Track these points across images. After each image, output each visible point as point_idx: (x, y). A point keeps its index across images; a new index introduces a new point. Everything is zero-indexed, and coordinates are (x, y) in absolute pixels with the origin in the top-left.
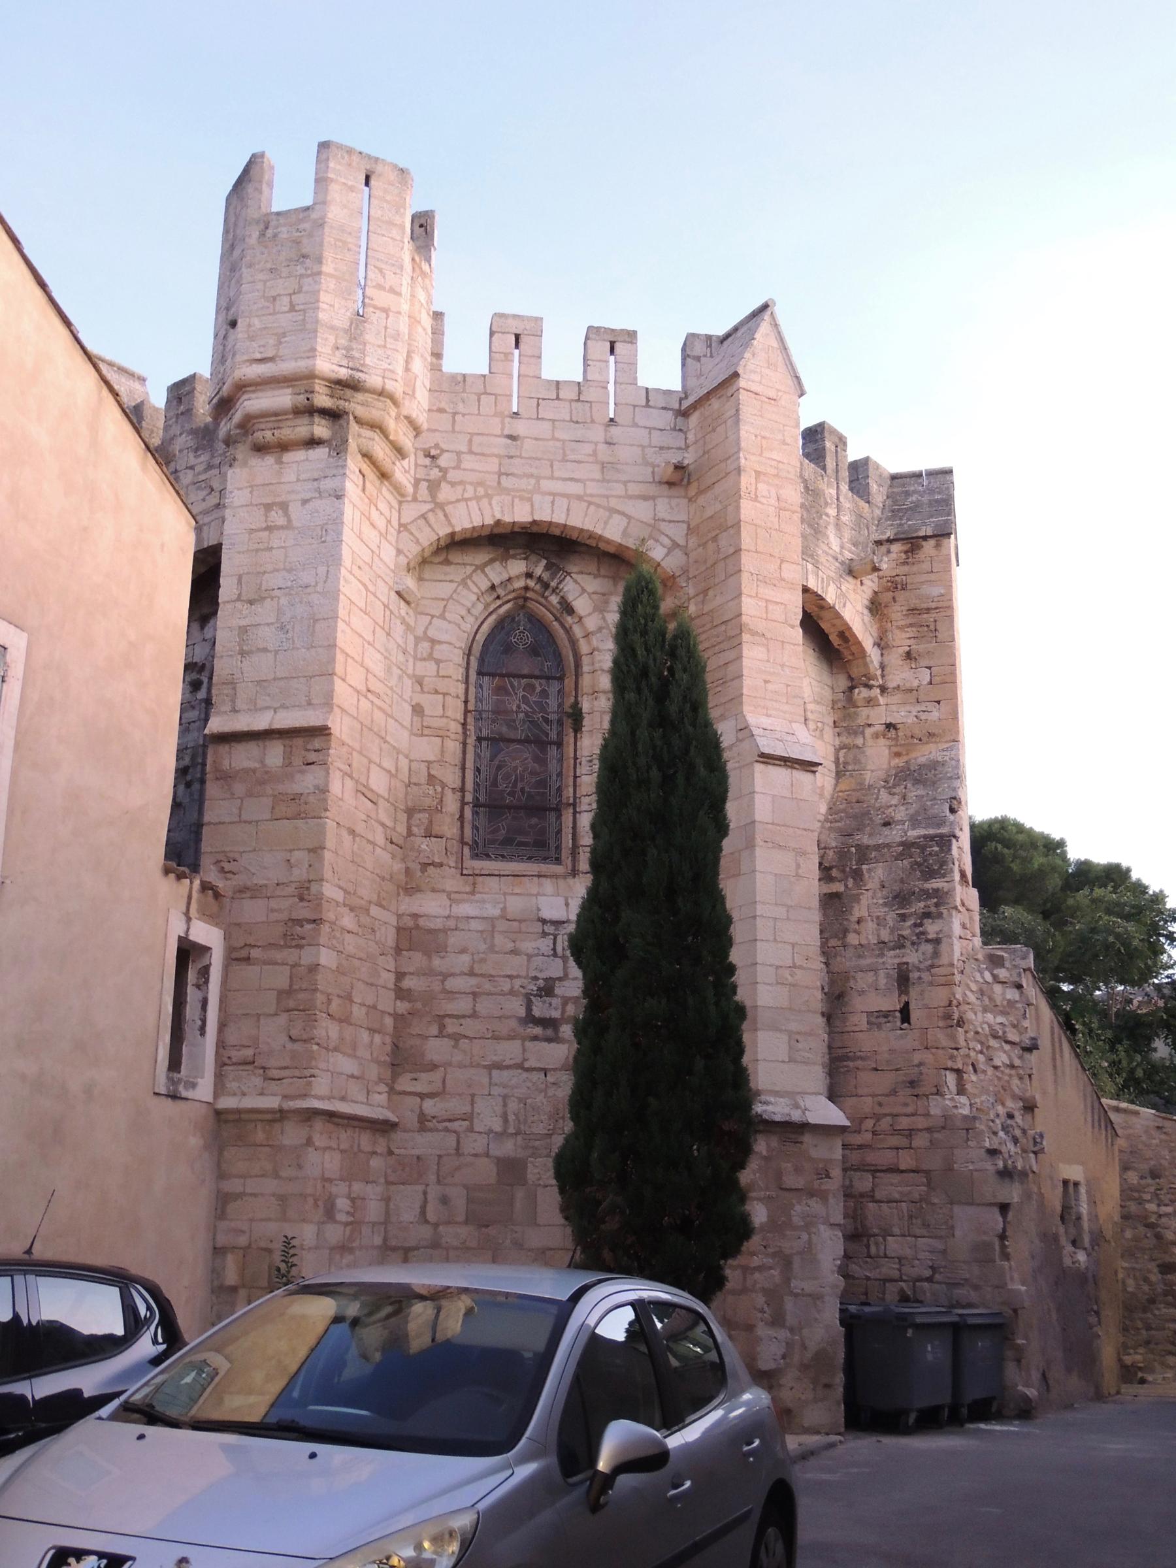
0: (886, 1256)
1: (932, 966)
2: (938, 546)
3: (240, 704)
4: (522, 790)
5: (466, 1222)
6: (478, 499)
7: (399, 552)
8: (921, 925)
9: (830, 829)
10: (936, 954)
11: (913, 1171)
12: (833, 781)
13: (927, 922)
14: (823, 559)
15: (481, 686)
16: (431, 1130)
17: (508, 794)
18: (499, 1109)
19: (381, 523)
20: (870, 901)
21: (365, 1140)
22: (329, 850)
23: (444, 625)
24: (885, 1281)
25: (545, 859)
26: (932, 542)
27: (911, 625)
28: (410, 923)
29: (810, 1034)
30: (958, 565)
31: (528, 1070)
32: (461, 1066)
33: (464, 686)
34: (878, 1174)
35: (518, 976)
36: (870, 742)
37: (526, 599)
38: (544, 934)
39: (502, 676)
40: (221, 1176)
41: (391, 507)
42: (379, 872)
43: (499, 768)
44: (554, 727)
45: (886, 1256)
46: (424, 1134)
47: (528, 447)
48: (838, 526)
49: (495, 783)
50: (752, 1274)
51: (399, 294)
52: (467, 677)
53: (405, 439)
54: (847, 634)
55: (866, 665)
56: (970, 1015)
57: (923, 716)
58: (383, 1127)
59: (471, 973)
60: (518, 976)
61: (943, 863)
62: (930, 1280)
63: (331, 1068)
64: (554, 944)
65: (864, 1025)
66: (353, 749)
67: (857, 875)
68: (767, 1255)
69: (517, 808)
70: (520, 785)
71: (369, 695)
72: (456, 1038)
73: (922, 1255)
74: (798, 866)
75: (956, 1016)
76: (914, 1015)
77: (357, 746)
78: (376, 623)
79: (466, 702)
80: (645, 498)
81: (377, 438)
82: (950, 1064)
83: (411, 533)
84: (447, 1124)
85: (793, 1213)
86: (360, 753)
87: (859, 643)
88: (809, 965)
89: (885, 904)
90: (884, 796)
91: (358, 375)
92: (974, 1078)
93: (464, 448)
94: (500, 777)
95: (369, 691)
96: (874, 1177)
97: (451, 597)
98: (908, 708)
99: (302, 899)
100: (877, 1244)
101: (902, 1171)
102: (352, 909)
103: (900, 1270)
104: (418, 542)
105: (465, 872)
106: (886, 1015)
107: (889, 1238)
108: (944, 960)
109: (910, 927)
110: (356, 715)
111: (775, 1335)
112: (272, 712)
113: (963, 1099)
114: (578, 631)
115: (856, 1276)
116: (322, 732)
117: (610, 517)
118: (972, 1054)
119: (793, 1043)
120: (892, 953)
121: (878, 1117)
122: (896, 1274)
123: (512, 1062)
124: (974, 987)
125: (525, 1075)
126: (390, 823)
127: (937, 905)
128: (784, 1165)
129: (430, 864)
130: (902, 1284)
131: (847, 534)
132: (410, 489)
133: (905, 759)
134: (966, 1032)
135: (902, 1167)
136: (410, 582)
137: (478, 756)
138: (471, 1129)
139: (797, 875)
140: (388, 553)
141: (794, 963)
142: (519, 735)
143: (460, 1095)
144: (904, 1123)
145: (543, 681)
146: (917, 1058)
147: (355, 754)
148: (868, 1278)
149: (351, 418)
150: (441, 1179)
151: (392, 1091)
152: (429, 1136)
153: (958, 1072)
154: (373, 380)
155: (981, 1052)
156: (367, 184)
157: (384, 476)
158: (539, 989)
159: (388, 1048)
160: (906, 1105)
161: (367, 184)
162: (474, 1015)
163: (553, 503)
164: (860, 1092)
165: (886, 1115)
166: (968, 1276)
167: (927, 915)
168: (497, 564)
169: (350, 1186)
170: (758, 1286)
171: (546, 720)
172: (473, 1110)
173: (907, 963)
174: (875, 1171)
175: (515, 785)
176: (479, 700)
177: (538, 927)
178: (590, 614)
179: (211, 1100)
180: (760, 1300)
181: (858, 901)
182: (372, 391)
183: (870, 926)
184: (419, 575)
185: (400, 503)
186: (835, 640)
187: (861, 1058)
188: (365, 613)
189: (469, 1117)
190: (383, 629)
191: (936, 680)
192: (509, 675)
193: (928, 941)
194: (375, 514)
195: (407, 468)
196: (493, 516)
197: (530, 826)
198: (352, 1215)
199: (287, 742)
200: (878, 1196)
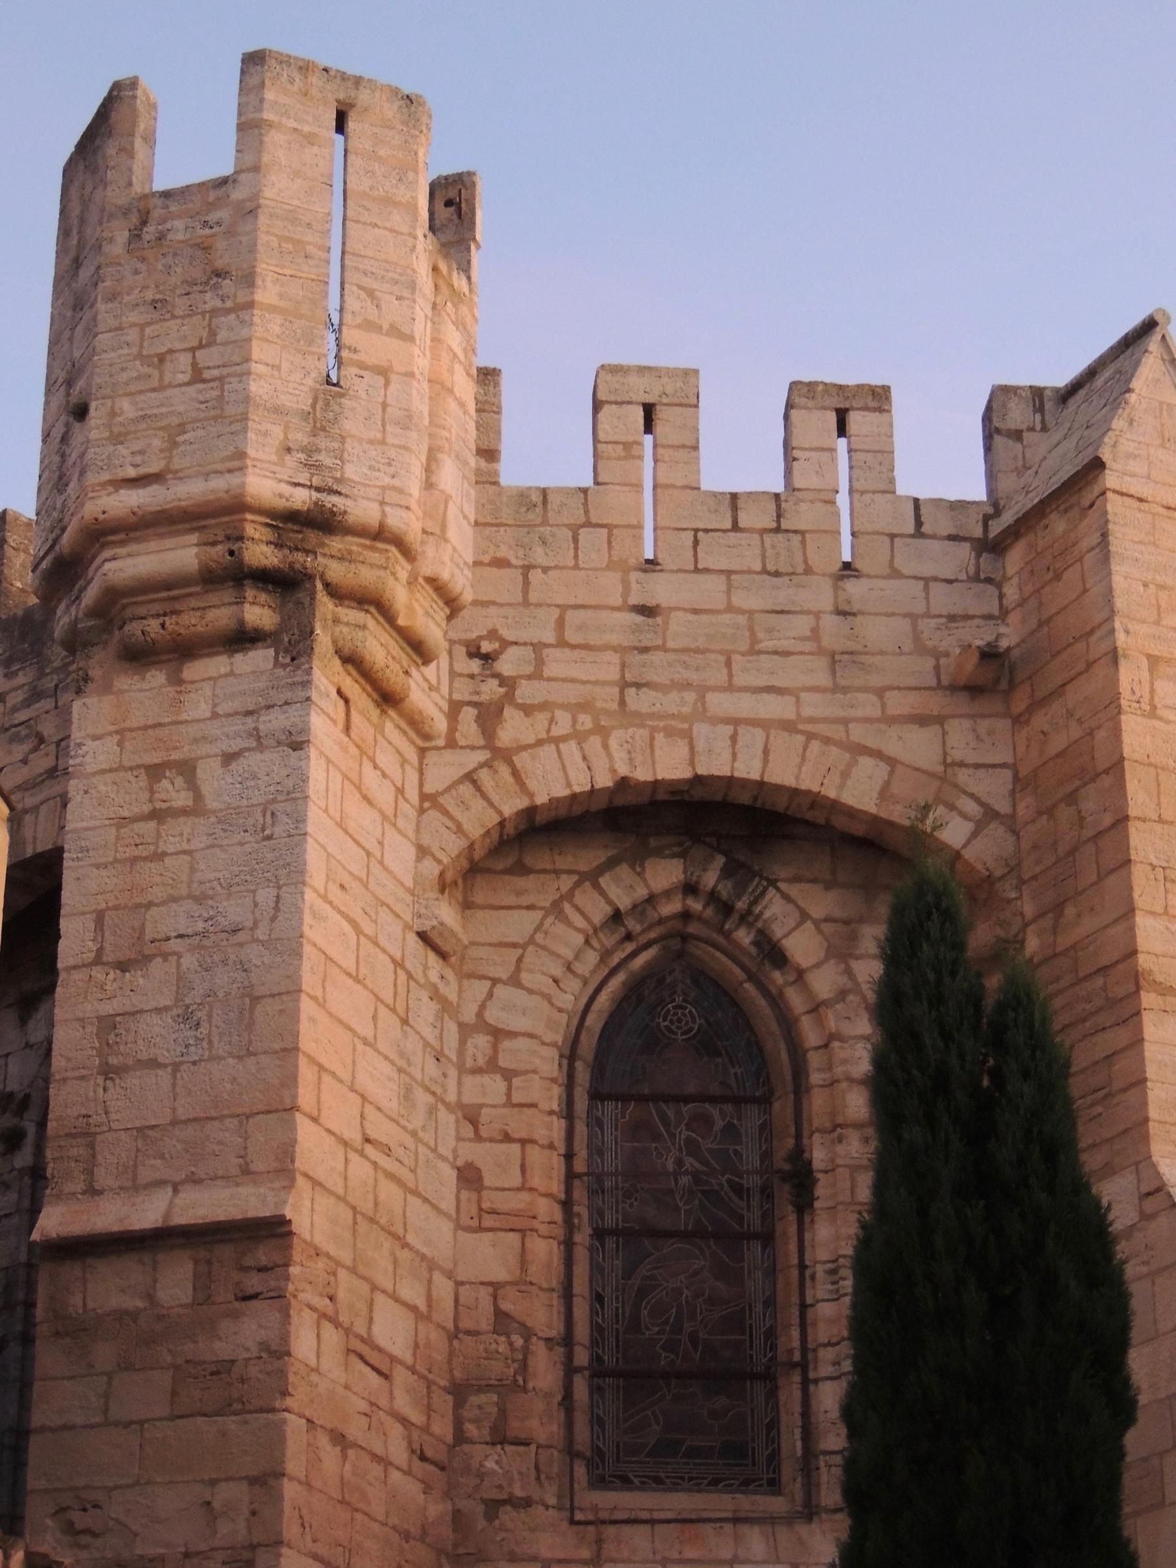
3: (104, 1177)
6: (580, 737)
7: (422, 852)
15: (599, 1123)
23: (516, 996)
25: (746, 1485)
37: (685, 938)
39: (642, 1099)
41: (404, 762)
44: (755, 1203)
70: (688, 1327)
71: (369, 1150)
77: (345, 1256)
79: (569, 1156)
80: (922, 720)
81: (371, 623)
83: (446, 813)
86: (353, 1270)
91: (330, 500)
93: (549, 637)
104: (459, 830)
114: (795, 1000)
126: (417, 1417)
129: (503, 1502)
132: (441, 724)
136: (446, 913)
145: (729, 1108)
161: (340, 128)
163: (734, 739)
168: (624, 870)
176: (595, 1150)
178: (818, 965)
182: (360, 532)
185: (422, 752)
194: (371, 777)
195: (434, 682)
196: (613, 771)
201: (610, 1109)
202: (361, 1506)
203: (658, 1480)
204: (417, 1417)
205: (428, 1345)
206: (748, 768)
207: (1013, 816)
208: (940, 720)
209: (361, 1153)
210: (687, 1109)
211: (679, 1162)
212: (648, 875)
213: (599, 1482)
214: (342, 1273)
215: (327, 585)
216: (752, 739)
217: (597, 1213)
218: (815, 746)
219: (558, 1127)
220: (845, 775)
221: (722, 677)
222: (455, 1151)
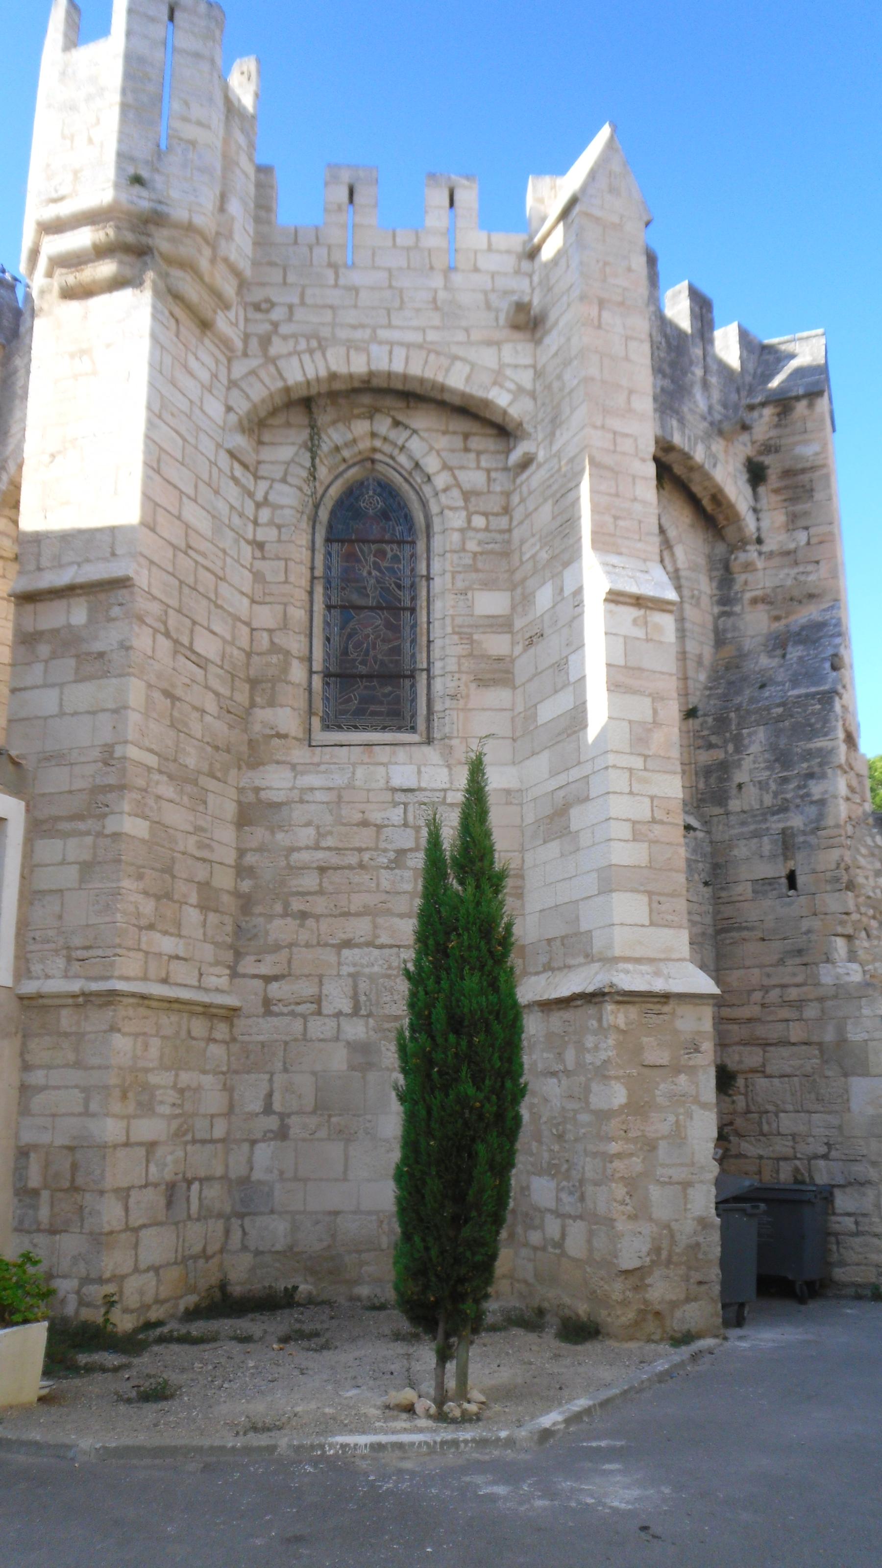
0: (779, 1134)
1: (818, 829)
2: (811, 406)
3: (45, 562)
4: (375, 657)
5: (314, 1112)
6: (311, 352)
7: (229, 409)
8: (805, 786)
9: (709, 696)
10: (821, 816)
11: (806, 1044)
12: (712, 650)
13: (811, 783)
14: (689, 417)
15: (330, 554)
16: (277, 1015)
17: (360, 663)
18: (349, 991)
19: (204, 376)
20: (752, 766)
21: (199, 1027)
22: (134, 710)
23: (285, 488)
24: (778, 1159)
25: (399, 729)
26: (804, 403)
27: (786, 488)
28: (251, 797)
29: (672, 895)
30: (834, 430)
31: (382, 947)
32: (307, 945)
33: (309, 552)
34: (769, 1048)
35: (367, 849)
36: (748, 609)
37: (373, 461)
38: (395, 804)
39: (351, 541)
40: (26, 1067)
41: (217, 361)
42: (209, 740)
43: (350, 636)
44: (407, 593)
45: (779, 1134)
46: (269, 1019)
47: (365, 298)
48: (705, 385)
49: (345, 652)
50: (611, 1162)
51: (209, 127)
52: (313, 542)
53: (229, 289)
54: (719, 497)
55: (740, 529)
56: (861, 880)
57: (802, 578)
58: (231, 1014)
59: (317, 847)
60: (367, 849)
61: (826, 721)
62: (825, 1157)
63: (144, 946)
64: (405, 813)
65: (749, 894)
66: (168, 606)
67: (738, 740)
68: (627, 1140)
69: (369, 677)
70: (372, 653)
71: (190, 552)
72: (303, 915)
73: (816, 1131)
74: (655, 712)
75: (845, 878)
76: (801, 880)
77: (174, 603)
78: (198, 477)
79: (312, 569)
80: (489, 343)
81: (188, 278)
82: (840, 930)
83: (242, 390)
84: (292, 1007)
85: (657, 1092)
86: (179, 611)
87: (731, 506)
88: (671, 820)
89: (767, 768)
90: (764, 661)
91: (160, 208)
92: (866, 944)
93: (296, 300)
94: (350, 646)
95: (190, 548)
96: (765, 1052)
97: (293, 460)
98: (786, 571)
99: (106, 764)
100: (769, 1123)
101: (794, 1044)
102: (171, 777)
103: (794, 1148)
104: (248, 397)
105: (313, 744)
106: (769, 882)
107: (782, 1115)
108: (830, 821)
109: (793, 790)
110: (170, 569)
111: (639, 1230)
112: (76, 567)
113: (855, 966)
114: (427, 490)
115: (749, 1154)
116: (122, 583)
117: (452, 364)
118: (865, 919)
119: (655, 905)
120: (776, 817)
121: (766, 989)
122: (789, 1152)
123: (362, 940)
124: (864, 851)
125: (376, 952)
126: (225, 691)
127: (821, 765)
128: (645, 1040)
129: (272, 736)
130: (797, 1162)
131: (716, 395)
132: (239, 344)
133: (783, 622)
134: (857, 896)
135: (793, 1040)
136: (239, 441)
137: (327, 624)
138: (319, 1013)
139: (654, 722)
140: (215, 408)
141: (653, 817)
142: (371, 602)
143: (307, 976)
144: (793, 994)
145: (395, 546)
146: (805, 925)
147: (171, 612)
148: (761, 1157)
149: (156, 253)
150: (288, 1066)
151: (234, 974)
152: (275, 1021)
153: (849, 937)
154: (180, 214)
155: (874, 917)
156: (171, 18)
157: (205, 325)
158: (391, 861)
159: (229, 928)
160: (794, 975)
161: (171, 18)
162: (321, 892)
163: (391, 353)
164: (748, 963)
165: (775, 986)
166: (865, 1152)
167: (811, 776)
168: (340, 426)
169: (177, 1075)
170: (618, 1175)
171: (399, 587)
172: (321, 992)
173: (792, 828)
174: (765, 1045)
175: (367, 653)
176: (328, 567)
177: (388, 796)
178: (438, 472)
179: (10, 984)
180: (620, 1191)
181: (739, 766)
182: (177, 226)
183: (752, 791)
184: (259, 436)
185: (229, 360)
186: (706, 502)
187: (747, 929)
188: (182, 464)
189: (318, 1000)
190: (209, 485)
191: (814, 541)
192: (358, 541)
193: (812, 802)
194: (193, 364)
195: (234, 320)
196: (328, 368)
197: (385, 695)
198: (181, 1106)
199: (92, 598)
200: (769, 1070)
201: (336, 546)
202: (184, 729)
203: (356, 727)
204: (225, 691)
205: (231, 656)
206: (398, 367)
207: (534, 391)
208: (498, 344)
209: (186, 553)
210: (374, 547)
211: (370, 573)
212: (352, 427)
213: (326, 727)
214: (171, 612)
215: (161, 254)
216: (400, 354)
217: (328, 597)
218: (432, 357)
219: (305, 554)
220: (448, 370)
221: (385, 321)
222: (251, 564)
